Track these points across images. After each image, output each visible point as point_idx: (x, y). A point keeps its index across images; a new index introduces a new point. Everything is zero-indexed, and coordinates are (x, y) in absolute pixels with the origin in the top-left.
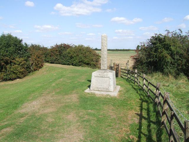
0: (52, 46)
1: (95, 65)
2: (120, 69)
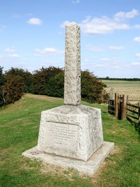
0: (37, 71)
1: (95, 98)
2: (125, 104)
